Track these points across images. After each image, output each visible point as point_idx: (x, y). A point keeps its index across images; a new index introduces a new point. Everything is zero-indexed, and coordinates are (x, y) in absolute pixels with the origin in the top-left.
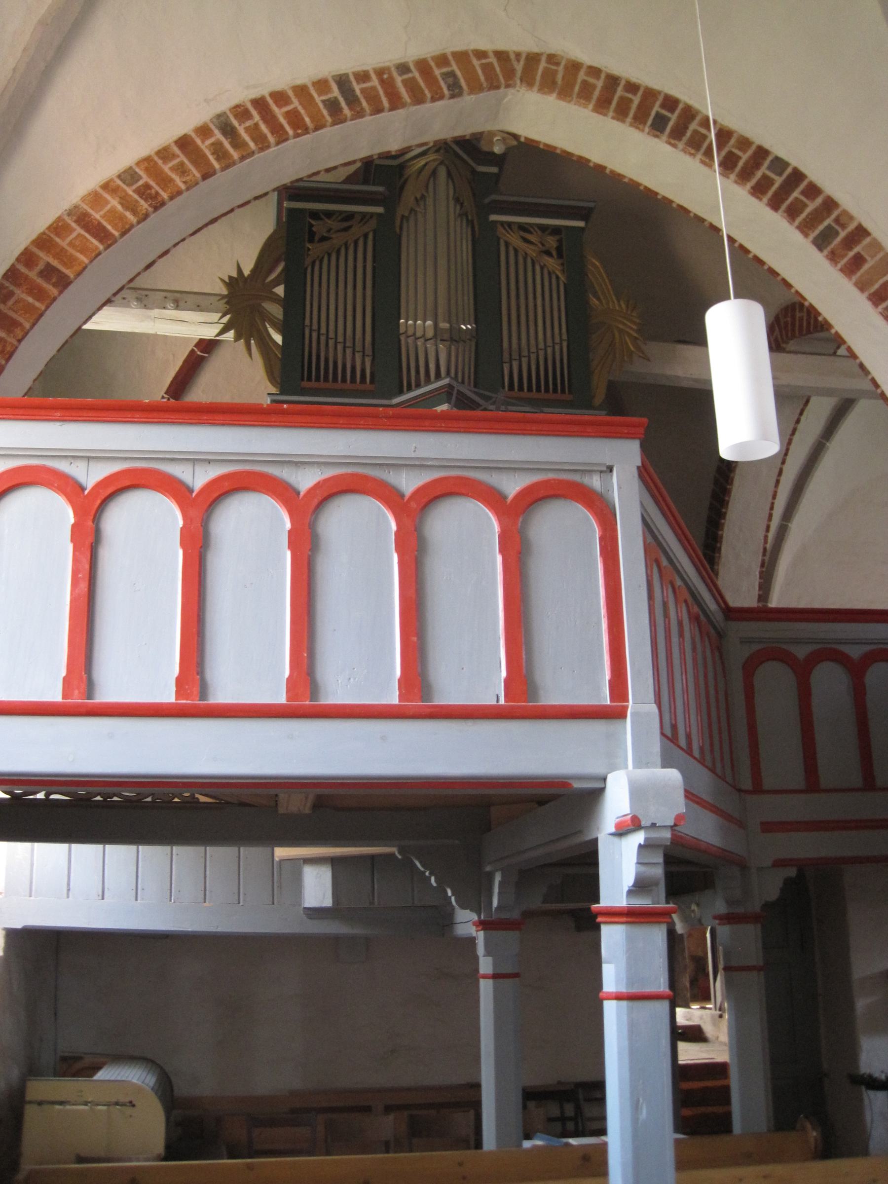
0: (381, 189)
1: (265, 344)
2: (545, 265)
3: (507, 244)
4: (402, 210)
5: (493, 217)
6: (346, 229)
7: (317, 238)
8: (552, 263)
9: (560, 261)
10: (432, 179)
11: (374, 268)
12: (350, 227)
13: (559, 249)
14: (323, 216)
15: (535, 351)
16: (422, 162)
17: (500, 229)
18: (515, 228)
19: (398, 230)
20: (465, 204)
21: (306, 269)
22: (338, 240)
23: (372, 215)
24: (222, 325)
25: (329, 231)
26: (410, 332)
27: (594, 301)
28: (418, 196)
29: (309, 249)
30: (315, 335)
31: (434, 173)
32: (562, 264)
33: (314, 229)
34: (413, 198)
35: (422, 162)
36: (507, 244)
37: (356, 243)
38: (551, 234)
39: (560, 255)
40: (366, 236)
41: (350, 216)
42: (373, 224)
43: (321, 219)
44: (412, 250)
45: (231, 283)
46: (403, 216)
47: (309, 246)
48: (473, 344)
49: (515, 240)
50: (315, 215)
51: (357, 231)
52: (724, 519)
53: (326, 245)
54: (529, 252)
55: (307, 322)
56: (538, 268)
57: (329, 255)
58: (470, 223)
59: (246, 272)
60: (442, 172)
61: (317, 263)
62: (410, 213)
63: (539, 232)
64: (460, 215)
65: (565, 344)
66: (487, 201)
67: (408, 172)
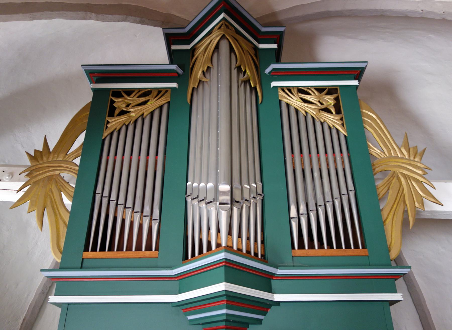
2: (325, 121)
3: (288, 105)
4: (192, 84)
5: (274, 84)
7: (117, 112)
8: (332, 119)
17: (281, 93)
18: (295, 91)
21: (104, 141)
22: (134, 113)
29: (108, 122)
30: (105, 201)
32: (341, 119)
33: (115, 105)
37: (152, 113)
39: (338, 112)
40: (161, 108)
41: (147, 93)
47: (107, 119)
49: (295, 101)
50: (117, 93)
51: (153, 104)
53: (123, 119)
54: (308, 110)
57: (127, 127)
63: (316, 93)
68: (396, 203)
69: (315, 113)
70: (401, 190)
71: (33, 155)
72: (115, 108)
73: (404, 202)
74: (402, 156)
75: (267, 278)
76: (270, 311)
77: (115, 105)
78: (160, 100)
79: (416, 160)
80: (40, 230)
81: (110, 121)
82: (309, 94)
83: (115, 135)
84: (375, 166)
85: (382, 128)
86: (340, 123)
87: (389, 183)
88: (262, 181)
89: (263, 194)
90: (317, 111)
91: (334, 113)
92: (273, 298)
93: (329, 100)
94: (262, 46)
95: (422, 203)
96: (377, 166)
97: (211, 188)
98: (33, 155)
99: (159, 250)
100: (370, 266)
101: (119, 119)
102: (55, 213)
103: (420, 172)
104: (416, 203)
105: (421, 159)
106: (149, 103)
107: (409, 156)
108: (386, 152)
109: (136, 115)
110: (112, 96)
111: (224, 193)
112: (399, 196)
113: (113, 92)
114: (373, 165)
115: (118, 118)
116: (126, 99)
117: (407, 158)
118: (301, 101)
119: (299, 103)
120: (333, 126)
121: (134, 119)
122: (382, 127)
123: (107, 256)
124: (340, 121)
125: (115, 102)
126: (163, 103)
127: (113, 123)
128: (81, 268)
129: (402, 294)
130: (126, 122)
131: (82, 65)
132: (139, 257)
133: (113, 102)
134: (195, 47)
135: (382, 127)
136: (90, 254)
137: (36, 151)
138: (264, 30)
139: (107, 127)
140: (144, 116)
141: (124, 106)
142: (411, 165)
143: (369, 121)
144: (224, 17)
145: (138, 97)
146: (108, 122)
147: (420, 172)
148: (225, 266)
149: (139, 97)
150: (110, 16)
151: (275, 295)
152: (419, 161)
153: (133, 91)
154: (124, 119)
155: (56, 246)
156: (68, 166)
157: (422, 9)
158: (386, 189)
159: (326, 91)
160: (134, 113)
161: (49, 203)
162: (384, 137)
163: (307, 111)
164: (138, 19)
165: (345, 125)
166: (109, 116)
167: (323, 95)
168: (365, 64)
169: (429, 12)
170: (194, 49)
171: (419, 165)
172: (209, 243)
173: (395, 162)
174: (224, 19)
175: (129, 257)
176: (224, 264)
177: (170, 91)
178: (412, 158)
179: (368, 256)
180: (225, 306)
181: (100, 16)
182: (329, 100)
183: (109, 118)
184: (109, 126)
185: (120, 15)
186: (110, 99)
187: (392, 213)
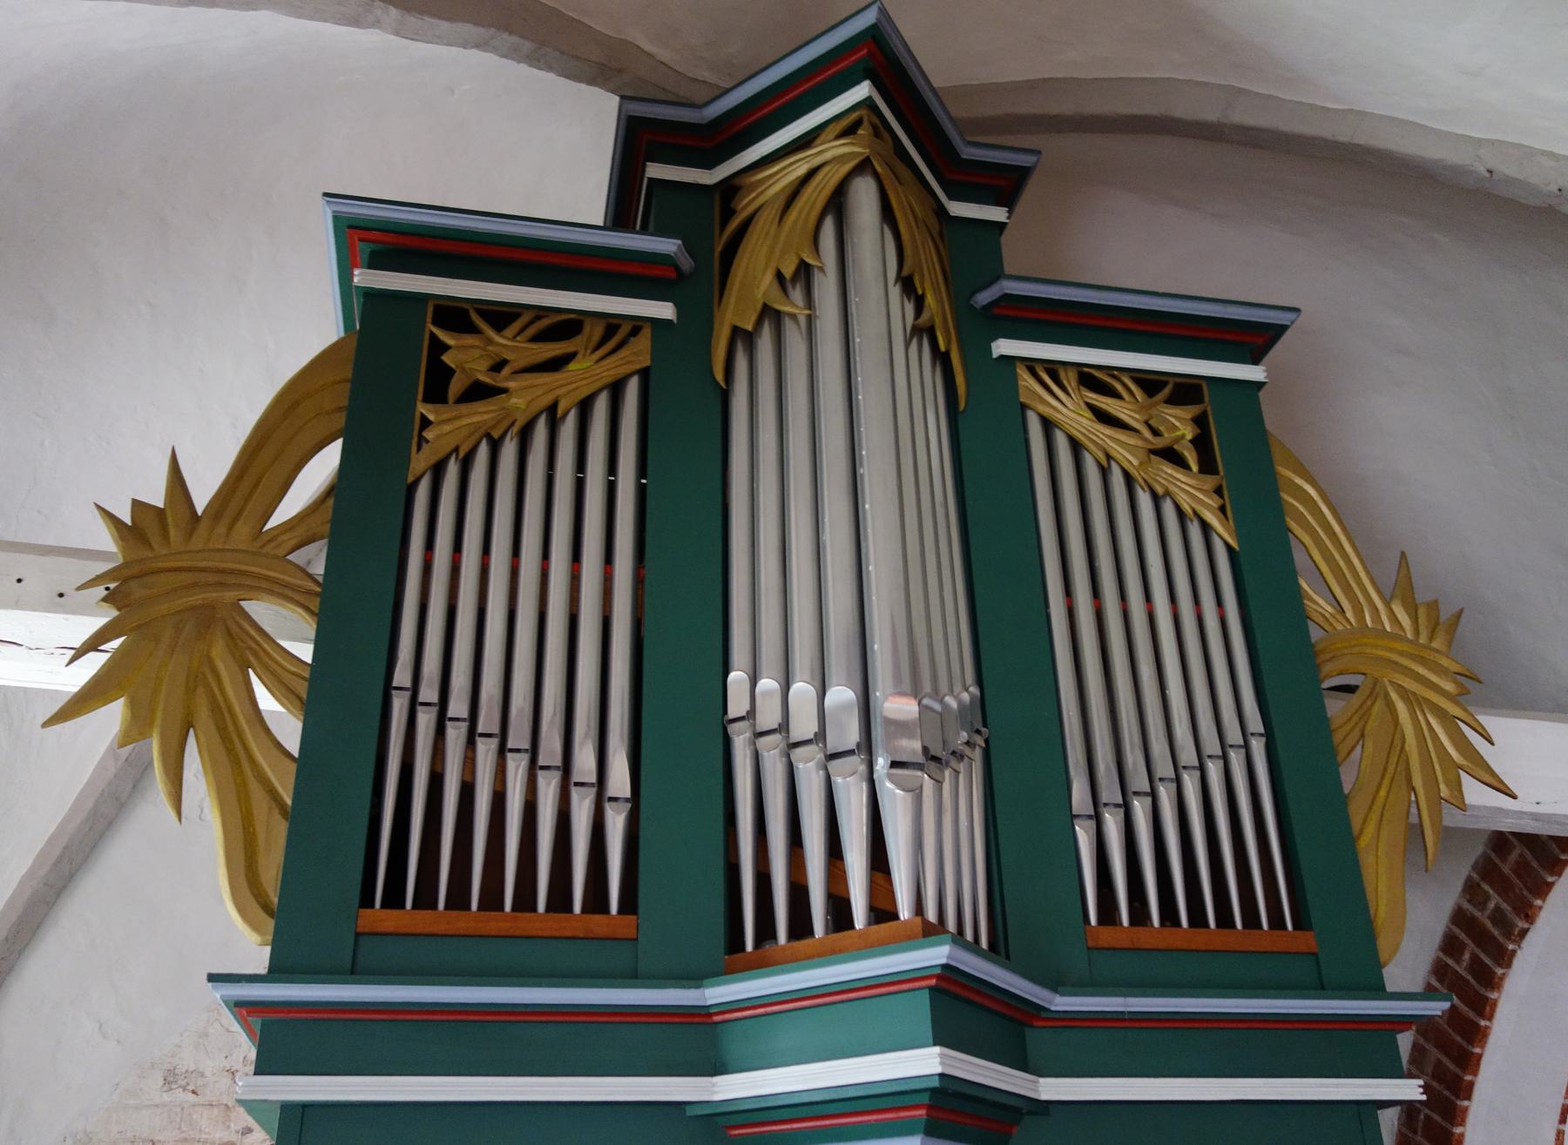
0: (667, 246)
1: (234, 740)
2: (1168, 493)
3: (1048, 425)
4: (735, 311)
5: (1004, 347)
6: (554, 365)
7: (456, 387)
8: (1189, 488)
9: (1210, 482)
10: (829, 226)
11: (642, 493)
12: (569, 358)
13: (1202, 443)
14: (475, 317)
15: (1171, 774)
16: (798, 167)
17: (1026, 380)
18: (1070, 378)
19: (720, 377)
20: (930, 299)
21: (411, 489)
22: (525, 395)
23: (637, 325)
24: (108, 656)
25: (497, 367)
26: (769, 717)
27: (1319, 604)
28: (788, 272)
29: (426, 423)
30: (425, 720)
31: (837, 204)
32: (1218, 491)
33: (446, 358)
34: (769, 277)
35: (798, 167)
36: (1048, 425)
37: (585, 407)
38: (1172, 401)
39: (1207, 466)
40: (616, 390)
41: (568, 326)
42: (639, 352)
43: (474, 330)
44: (768, 437)
45: (141, 529)
46: (736, 331)
47: (423, 409)
48: (977, 754)
49: (1071, 411)
50: (454, 315)
51: (587, 371)
52: (1469, 1097)
53: (482, 413)
55: (402, 676)
56: (1144, 500)
57: (495, 447)
58: (942, 359)
59: (202, 495)
60: (864, 195)
61: (453, 470)
62: (759, 323)
64: (917, 331)
65: (1258, 747)
66: (984, 298)
67: (745, 205)
68: (1386, 782)
69: (1135, 462)
70: (1398, 742)
71: (128, 521)
73: (1409, 779)
74: (1397, 631)
75: (1002, 1015)
76: (1016, 1131)
77: (446, 358)
79: (1434, 645)
80: (175, 819)
81: (431, 417)
82: (1117, 396)
83: (601, 408)
84: (1323, 657)
85: (1334, 534)
86: (1214, 502)
87: (1364, 714)
88: (980, 681)
89: (984, 730)
90: (1143, 454)
91: (1195, 468)
92: (1036, 1091)
93: (1179, 424)
94: (958, 209)
95: (1457, 786)
96: (1328, 656)
97: (844, 707)
98: (128, 521)
99: (641, 910)
100: (1323, 988)
101: (468, 415)
102: (230, 751)
103: (1449, 687)
104: (1442, 787)
105: (1449, 644)
106: (572, 366)
107: (1417, 632)
108: (1349, 614)
110: (434, 323)
111: (899, 727)
112: (1394, 759)
113: (437, 308)
114: (1316, 654)
115: (464, 408)
116: (490, 341)
117: (1410, 635)
118: (1088, 414)
119: (1084, 421)
120: (1195, 512)
121: (521, 421)
122: (1337, 528)
123: (441, 928)
124: (1216, 497)
125: (446, 348)
127: (447, 428)
128: (352, 973)
129: (1421, 1082)
130: (494, 427)
131: (326, 195)
132: (569, 933)
133: (438, 347)
134: (738, 181)
135: (1337, 528)
136: (378, 917)
137: (136, 504)
138: (968, 153)
139: (422, 440)
140: (560, 412)
141: (484, 365)
142: (1423, 661)
143: (1301, 508)
144: (869, 98)
146: (426, 423)
147: (1449, 687)
148: (931, 988)
149: (536, 339)
150: (444, 25)
151: (1042, 1080)
152: (1444, 649)
153: (516, 316)
154: (486, 417)
155: (242, 880)
157: (1489, 166)
158: (1357, 732)
159: (1167, 391)
161: (203, 715)
162: (1342, 563)
163: (1113, 453)
164: (527, 46)
165: (1229, 513)
166: (428, 399)
167: (1157, 403)
168: (1289, 316)
169: (1510, 181)
170: (729, 189)
171: (1445, 662)
172: (799, 893)
173: (1377, 647)
174: (868, 103)
175: (534, 933)
176: (933, 982)
177: (646, 332)
178: (1422, 640)
179: (1314, 954)
180: (922, 1127)
181: (413, 20)
183: (430, 406)
184: (429, 434)
185: (476, 24)
186: (427, 337)
187: (1374, 817)
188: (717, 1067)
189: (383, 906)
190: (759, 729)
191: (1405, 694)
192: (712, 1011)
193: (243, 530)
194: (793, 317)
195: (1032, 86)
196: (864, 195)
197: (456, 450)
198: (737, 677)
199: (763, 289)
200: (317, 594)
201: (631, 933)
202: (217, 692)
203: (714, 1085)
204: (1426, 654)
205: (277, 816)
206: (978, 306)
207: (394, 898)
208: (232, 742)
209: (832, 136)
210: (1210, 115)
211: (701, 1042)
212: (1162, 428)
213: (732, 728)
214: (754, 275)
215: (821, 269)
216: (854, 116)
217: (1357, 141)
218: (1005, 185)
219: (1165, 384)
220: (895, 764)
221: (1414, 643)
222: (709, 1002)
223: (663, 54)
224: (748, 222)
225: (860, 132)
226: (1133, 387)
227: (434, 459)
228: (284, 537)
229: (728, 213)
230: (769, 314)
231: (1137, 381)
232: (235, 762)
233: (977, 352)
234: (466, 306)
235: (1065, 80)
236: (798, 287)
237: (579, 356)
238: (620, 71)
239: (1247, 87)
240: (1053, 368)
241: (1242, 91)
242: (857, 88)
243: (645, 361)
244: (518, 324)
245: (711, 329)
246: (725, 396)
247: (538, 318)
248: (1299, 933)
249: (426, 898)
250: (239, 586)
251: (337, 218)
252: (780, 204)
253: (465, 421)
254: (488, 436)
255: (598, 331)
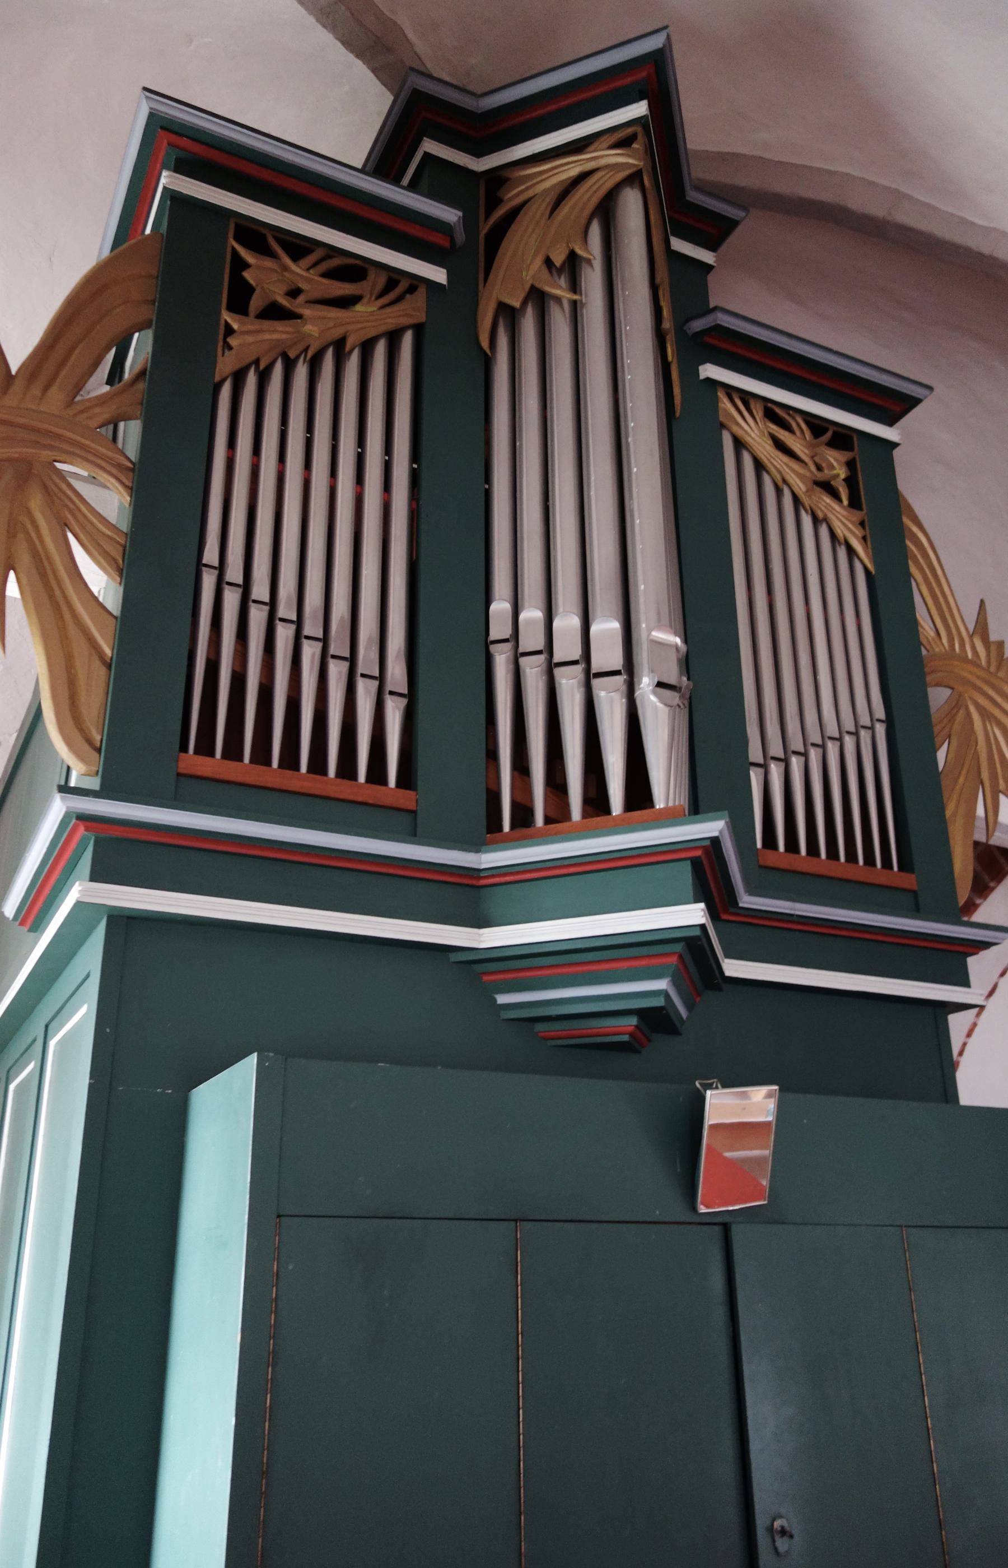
0: (450, 215)
2: (826, 520)
3: (739, 444)
4: (505, 287)
5: (710, 371)
6: (345, 302)
7: (256, 303)
8: (842, 519)
9: (857, 515)
13: (851, 481)
16: (571, 167)
19: (485, 344)
21: (218, 387)
23: (416, 282)
27: (926, 629)
29: (229, 331)
30: (231, 600)
31: (606, 211)
32: (862, 524)
33: (247, 275)
34: (539, 262)
35: (571, 167)
36: (739, 444)
37: (367, 348)
39: (855, 503)
40: (393, 338)
41: (355, 269)
42: (413, 309)
47: (226, 316)
50: (254, 235)
51: (368, 316)
53: (278, 332)
55: (211, 555)
60: (632, 208)
62: (524, 304)
65: (880, 730)
66: (698, 325)
67: (512, 196)
72: (250, 290)
78: (388, 310)
81: (235, 326)
83: (380, 351)
86: (859, 532)
91: (846, 502)
104: (1001, 782)
106: (359, 307)
107: (989, 662)
108: (945, 640)
109: (321, 332)
115: (267, 324)
116: (285, 268)
117: (984, 663)
118: (770, 442)
125: (246, 266)
126: (405, 321)
127: (250, 339)
130: (290, 347)
131: (145, 89)
132: (360, 799)
133: (239, 265)
136: (191, 761)
142: (993, 687)
145: (326, 275)
149: (328, 275)
156: (88, 442)
160: (317, 325)
161: (24, 558)
167: (818, 445)
168: (926, 392)
170: (497, 180)
178: (992, 669)
182: (835, 464)
184: (233, 341)
188: (481, 921)
189: (197, 752)
190: (521, 650)
191: (979, 708)
192: (482, 874)
193: (56, 395)
194: (558, 300)
195: (724, 158)
196: (632, 208)
197: (257, 362)
198: (500, 606)
199: (531, 272)
200: (127, 469)
201: (412, 806)
202: (37, 542)
203: (480, 935)
204: (995, 681)
205: (97, 663)
206: (690, 333)
207: (205, 747)
208: (53, 590)
209: (606, 145)
210: (876, 209)
211: (468, 897)
212: (824, 465)
213: (493, 648)
214: (523, 260)
215: (589, 262)
216: (630, 130)
217: (995, 255)
218: (714, 231)
219: (826, 430)
220: (660, 685)
221: (987, 670)
222: (483, 866)
223: (421, 48)
224: (514, 213)
225: (635, 146)
226: (804, 426)
227: (237, 367)
228: (97, 410)
229: (493, 201)
230: (538, 298)
231: (807, 423)
232: (56, 607)
233: (690, 371)
234: (264, 231)
235: (753, 157)
236: (563, 277)
237: (365, 300)
238: (389, 50)
239: (910, 192)
240: (746, 397)
241: (909, 198)
242: (635, 106)
243: (421, 317)
244: (310, 259)
245: (476, 304)
246: (488, 363)
247: (328, 257)
248: (902, 874)
249: (233, 751)
250: (52, 448)
251: (153, 117)
252: (552, 197)
253: (267, 336)
254: (285, 356)
255: (381, 281)
